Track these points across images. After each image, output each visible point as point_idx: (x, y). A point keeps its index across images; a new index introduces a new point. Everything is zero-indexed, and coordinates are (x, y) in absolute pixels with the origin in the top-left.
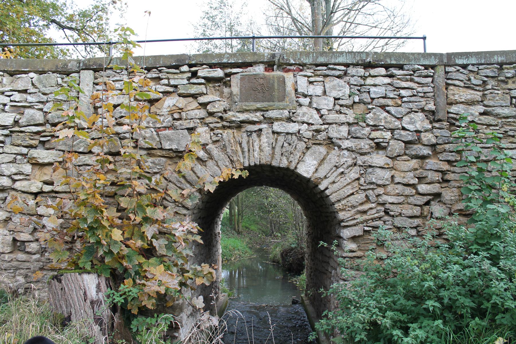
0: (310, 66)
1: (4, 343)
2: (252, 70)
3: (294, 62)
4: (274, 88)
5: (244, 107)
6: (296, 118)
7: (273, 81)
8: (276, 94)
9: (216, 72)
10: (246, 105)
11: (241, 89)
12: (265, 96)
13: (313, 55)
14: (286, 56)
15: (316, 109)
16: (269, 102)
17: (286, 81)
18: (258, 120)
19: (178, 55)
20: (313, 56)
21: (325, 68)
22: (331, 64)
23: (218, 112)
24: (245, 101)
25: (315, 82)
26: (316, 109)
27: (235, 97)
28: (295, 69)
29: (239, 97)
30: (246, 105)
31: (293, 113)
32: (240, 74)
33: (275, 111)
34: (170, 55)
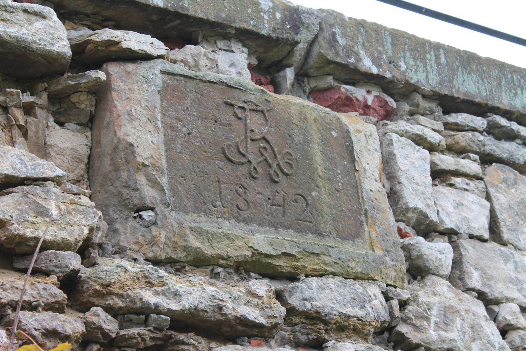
0: (424, 104)
1: (525, 272)
2: (203, 62)
3: (375, 70)
4: (313, 170)
5: (194, 242)
6: (416, 328)
7: (305, 132)
8: (325, 198)
9: (39, 24)
10: (199, 233)
11: (168, 143)
12: (279, 199)
13: (437, 57)
14: (344, 35)
15: (481, 296)
16: (300, 231)
17: (357, 147)
18: (261, 320)
19: (472, 53)
20: (438, 63)
21: (480, 122)
22: (496, 110)
23: (64, 246)
24: (197, 210)
25: (457, 174)
26: (481, 296)
27: (141, 179)
28: (370, 100)
29: (164, 181)
30: (199, 233)
31: (403, 304)
32: (159, 65)
33: (331, 281)
34: (465, 52)
